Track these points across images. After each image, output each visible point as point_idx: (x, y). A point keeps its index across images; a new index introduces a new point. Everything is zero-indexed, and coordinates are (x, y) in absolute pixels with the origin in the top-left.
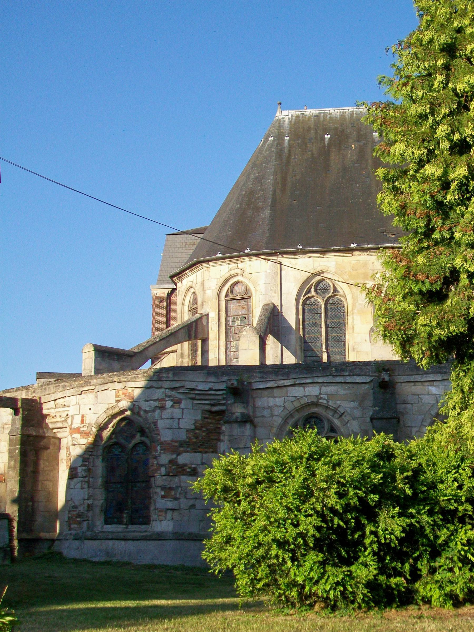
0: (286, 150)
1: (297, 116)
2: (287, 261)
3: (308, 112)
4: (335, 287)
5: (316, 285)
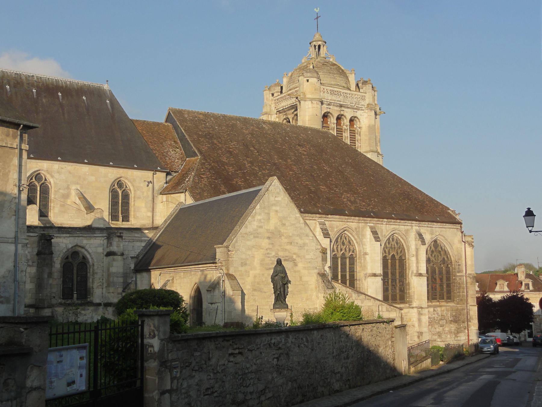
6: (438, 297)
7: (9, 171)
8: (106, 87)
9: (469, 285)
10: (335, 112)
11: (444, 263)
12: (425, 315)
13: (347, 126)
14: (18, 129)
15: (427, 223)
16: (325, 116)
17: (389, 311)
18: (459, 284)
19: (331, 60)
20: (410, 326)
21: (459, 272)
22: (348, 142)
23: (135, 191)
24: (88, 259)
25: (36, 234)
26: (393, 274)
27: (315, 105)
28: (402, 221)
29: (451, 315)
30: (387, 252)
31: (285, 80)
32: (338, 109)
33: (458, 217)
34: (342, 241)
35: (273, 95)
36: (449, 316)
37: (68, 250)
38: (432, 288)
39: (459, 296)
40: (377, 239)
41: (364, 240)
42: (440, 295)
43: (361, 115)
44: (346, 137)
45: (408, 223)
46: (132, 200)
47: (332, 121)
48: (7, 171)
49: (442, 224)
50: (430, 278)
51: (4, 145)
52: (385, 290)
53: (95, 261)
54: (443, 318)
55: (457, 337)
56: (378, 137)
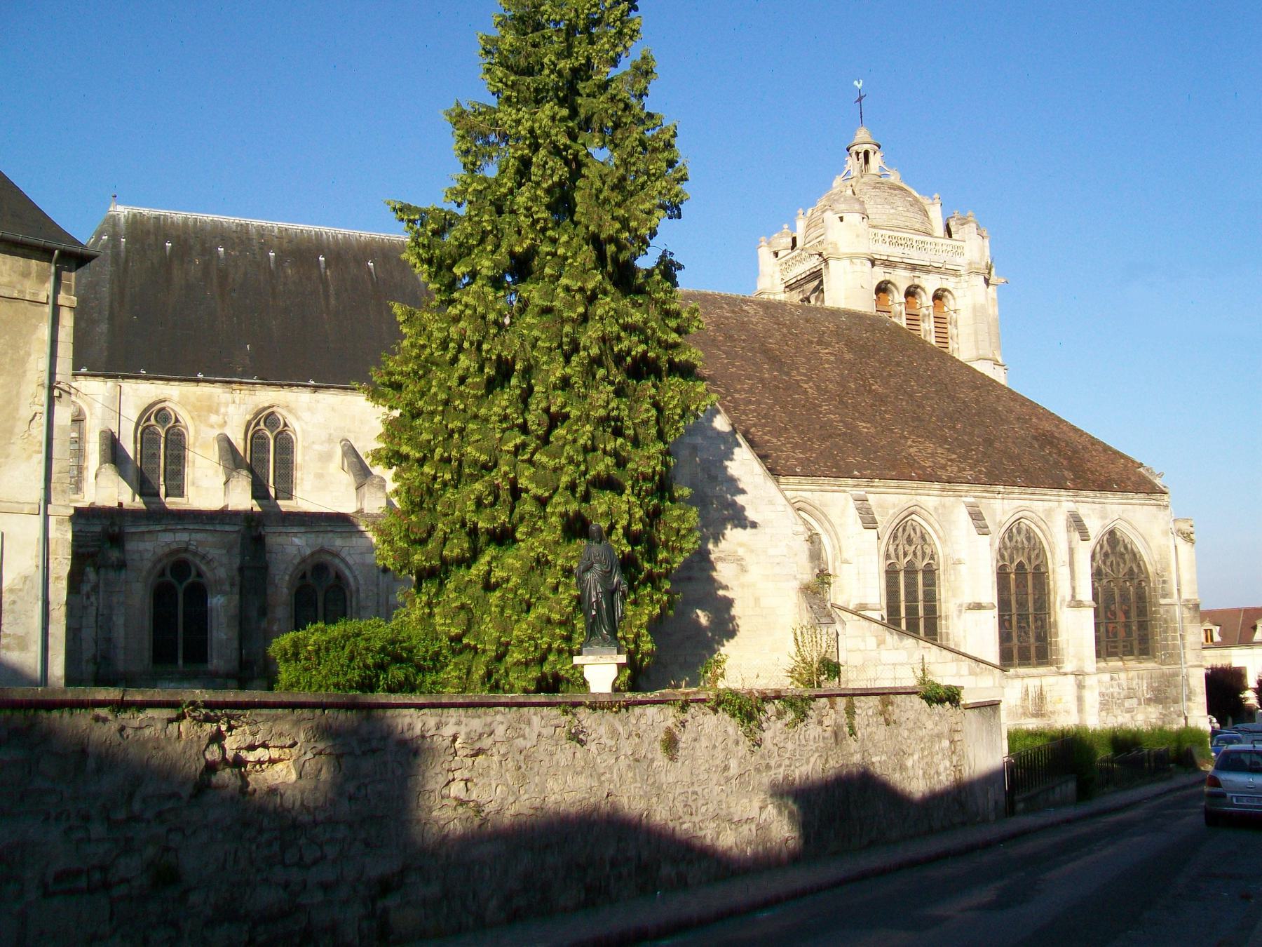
0: (123, 255)
1: (135, 215)
2: (129, 386)
3: (146, 211)
5: (157, 414)
7: (29, 354)
10: (902, 280)
14: (50, 261)
17: (976, 675)
18: (1166, 621)
21: (1164, 596)
22: (903, 323)
24: (346, 579)
25: (237, 528)
26: (1022, 604)
29: (1150, 687)
31: (801, 225)
32: (908, 274)
34: (906, 536)
35: (776, 254)
36: (1143, 688)
37: (304, 560)
39: (1166, 647)
40: (983, 530)
44: (928, 331)
47: (898, 297)
48: (22, 353)
50: (1102, 606)
51: (16, 295)
52: (1005, 637)
53: (361, 582)
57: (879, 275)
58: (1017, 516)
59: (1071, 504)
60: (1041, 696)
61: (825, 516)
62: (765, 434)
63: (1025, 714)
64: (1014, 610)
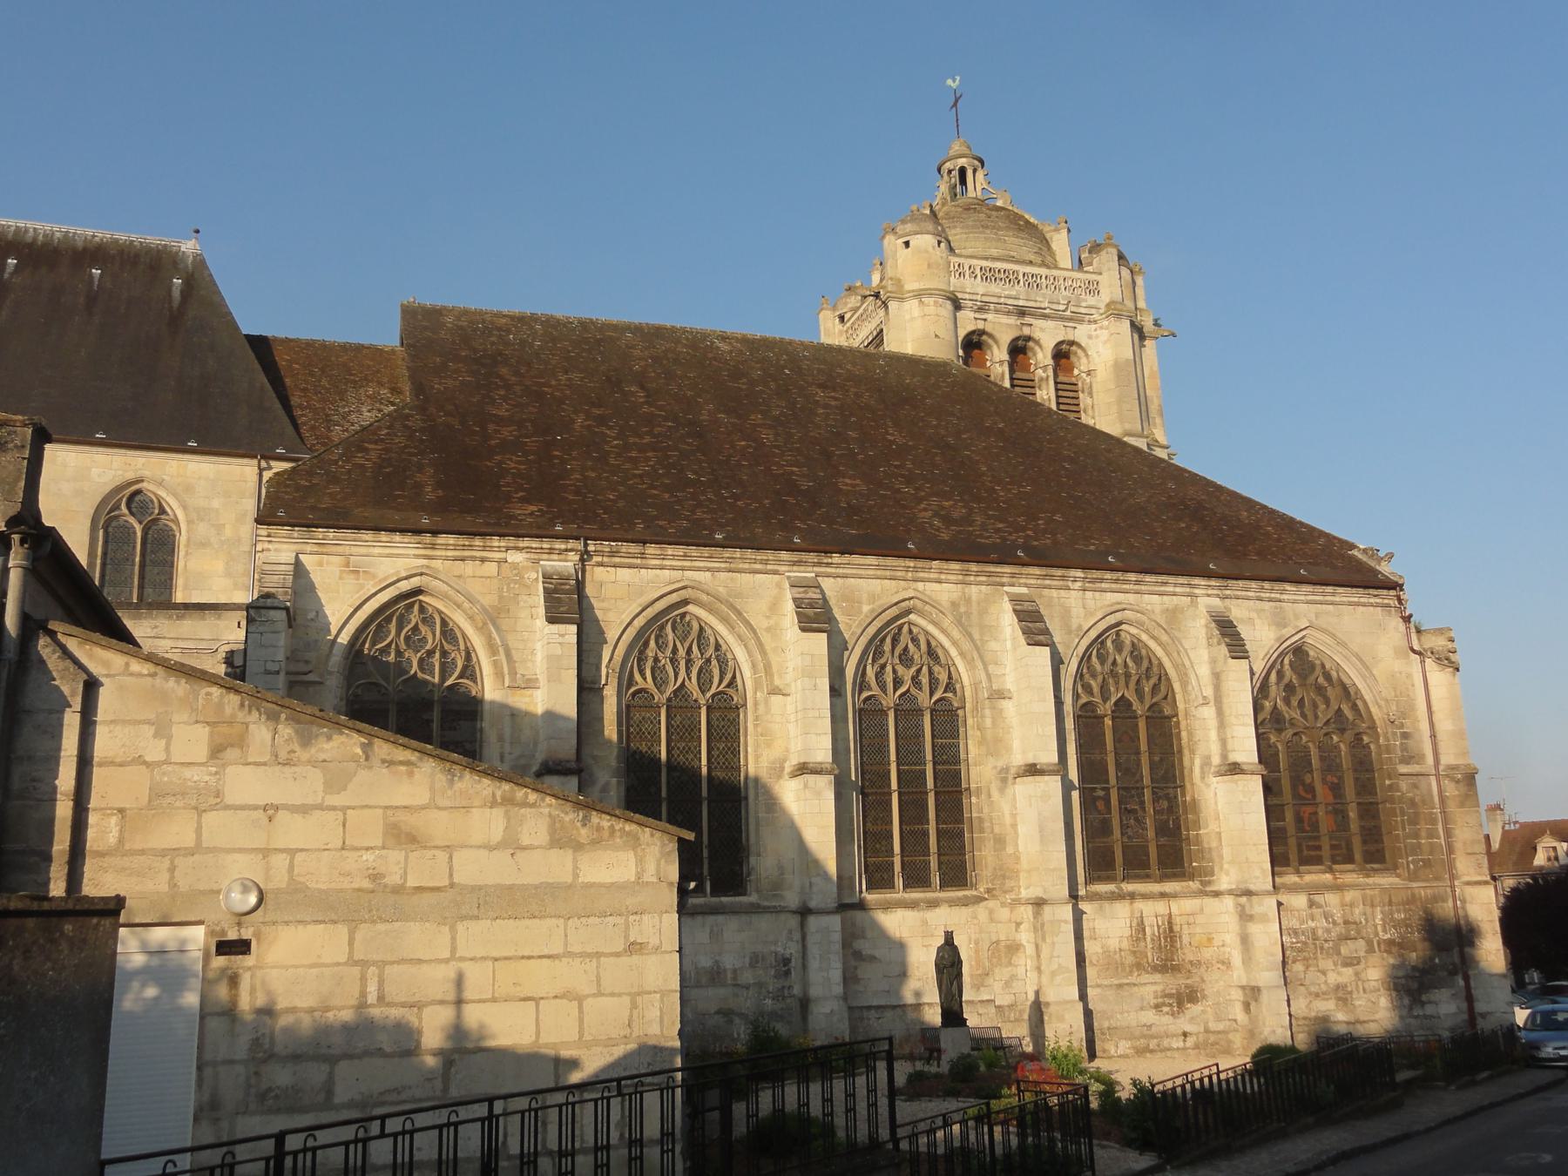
4: (161, 506)
6: (1326, 852)
8: (189, 247)
9: (1452, 807)
10: (1003, 329)
11: (1342, 731)
12: (1264, 919)
13: (1045, 368)
15: (1253, 584)
16: (974, 344)
17: (578, 847)
18: (1413, 803)
19: (999, 203)
20: (1208, 965)
21: (1407, 760)
23: (189, 522)
26: (1128, 770)
27: (931, 310)
28: (1148, 578)
29: (1388, 921)
30: (1096, 690)
32: (1012, 320)
33: (1385, 569)
35: (842, 318)
38: (1299, 819)
39: (1416, 849)
41: (993, 645)
42: (1333, 847)
43: (1090, 337)
44: (1046, 395)
45: (1176, 584)
46: (182, 554)
49: (1319, 589)
54: (1350, 930)
55: (1423, 1004)
56: (1156, 401)
57: (968, 322)
58: (1111, 620)
59: (1217, 601)
60: (1170, 934)
61: (739, 613)
62: (652, 487)
63: (1138, 966)
64: (1113, 781)
